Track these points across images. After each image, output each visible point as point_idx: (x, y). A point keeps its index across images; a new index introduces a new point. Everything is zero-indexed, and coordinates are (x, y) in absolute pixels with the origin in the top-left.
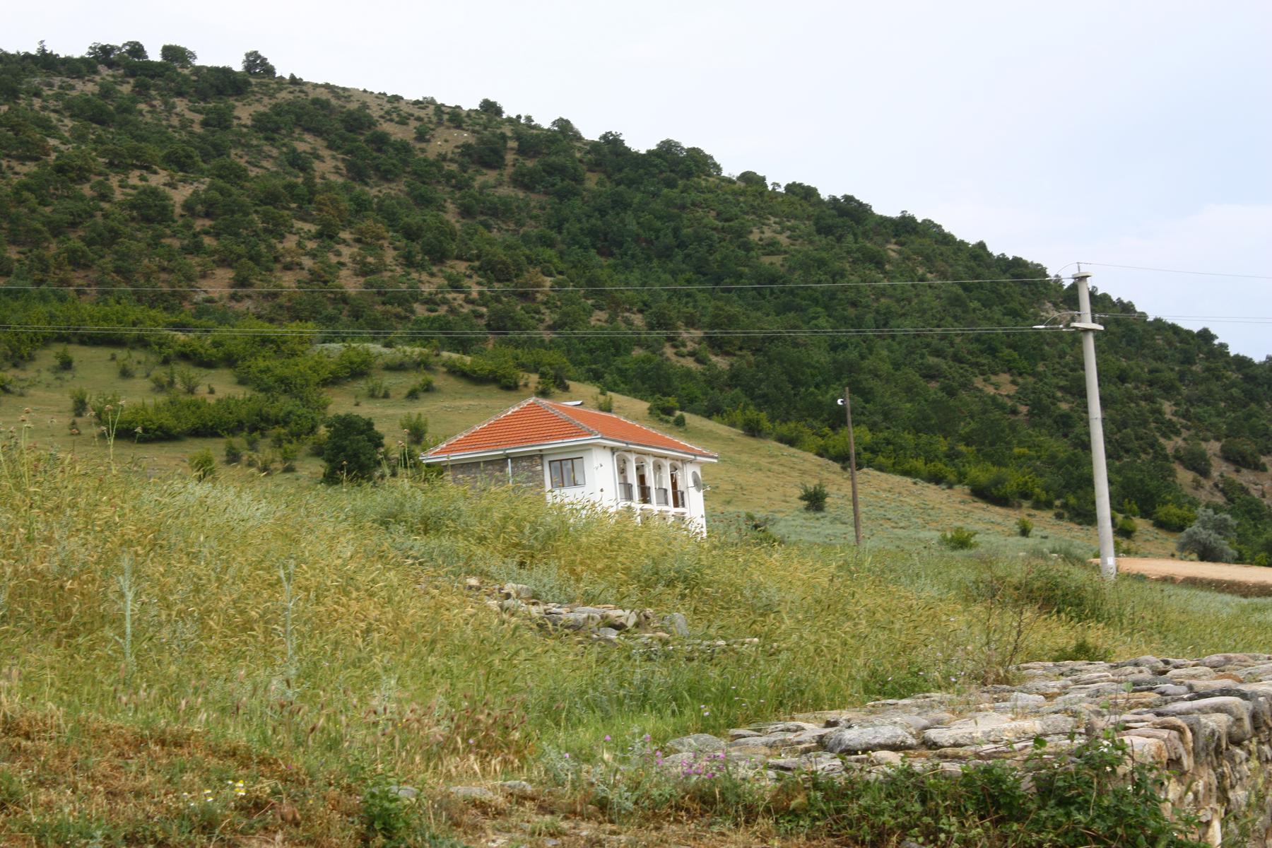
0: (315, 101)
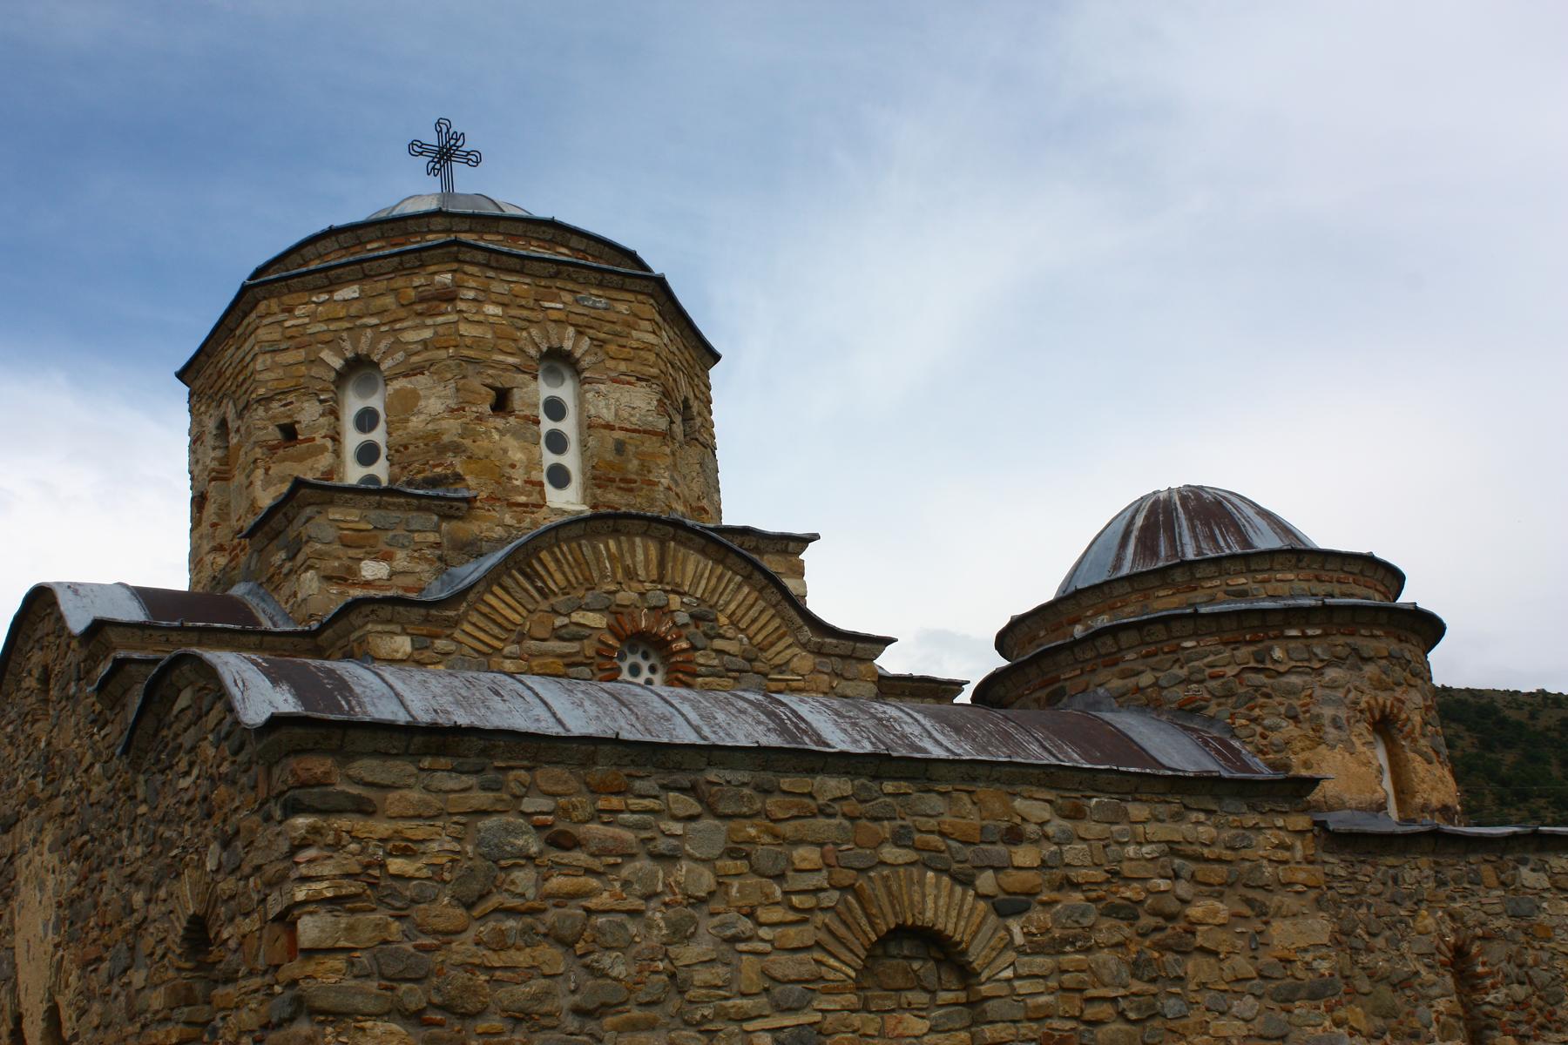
0: (1458, 701)
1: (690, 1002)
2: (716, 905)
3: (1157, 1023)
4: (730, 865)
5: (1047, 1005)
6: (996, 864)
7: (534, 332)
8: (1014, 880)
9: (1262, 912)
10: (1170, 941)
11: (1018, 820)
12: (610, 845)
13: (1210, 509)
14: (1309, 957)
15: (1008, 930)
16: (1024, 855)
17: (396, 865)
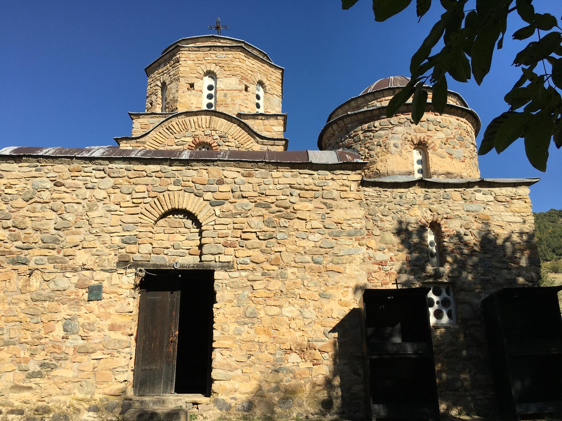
3: (273, 240)
5: (226, 233)
7: (203, 67)
8: (219, 196)
9: (330, 207)
10: (283, 215)
11: (223, 177)
12: (72, 185)
13: (505, 98)
14: (349, 222)
16: (223, 188)
17: (7, 191)
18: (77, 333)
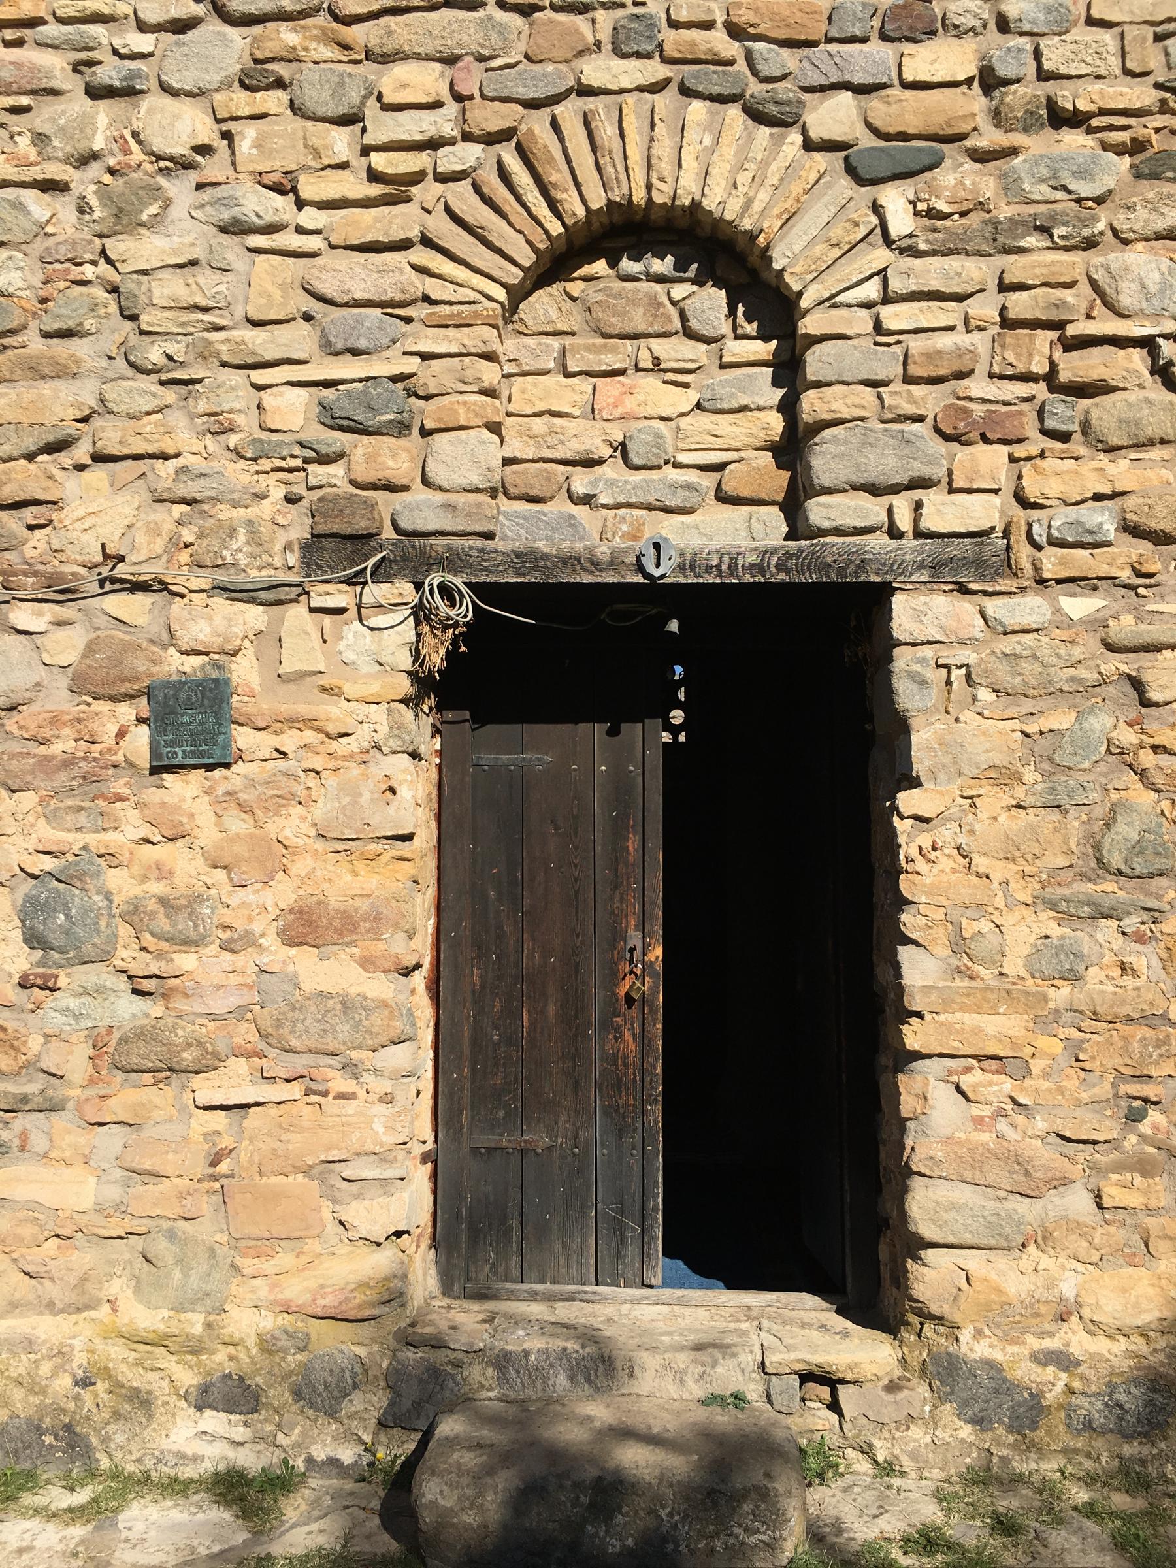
1: (142, 333)
2: (214, 168)
4: (241, 101)
5: (959, 352)
6: (858, 78)
8: (904, 111)
15: (876, 208)
18: (104, 957)
